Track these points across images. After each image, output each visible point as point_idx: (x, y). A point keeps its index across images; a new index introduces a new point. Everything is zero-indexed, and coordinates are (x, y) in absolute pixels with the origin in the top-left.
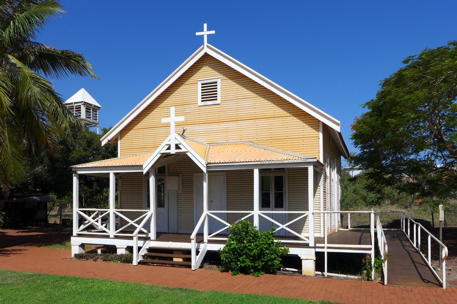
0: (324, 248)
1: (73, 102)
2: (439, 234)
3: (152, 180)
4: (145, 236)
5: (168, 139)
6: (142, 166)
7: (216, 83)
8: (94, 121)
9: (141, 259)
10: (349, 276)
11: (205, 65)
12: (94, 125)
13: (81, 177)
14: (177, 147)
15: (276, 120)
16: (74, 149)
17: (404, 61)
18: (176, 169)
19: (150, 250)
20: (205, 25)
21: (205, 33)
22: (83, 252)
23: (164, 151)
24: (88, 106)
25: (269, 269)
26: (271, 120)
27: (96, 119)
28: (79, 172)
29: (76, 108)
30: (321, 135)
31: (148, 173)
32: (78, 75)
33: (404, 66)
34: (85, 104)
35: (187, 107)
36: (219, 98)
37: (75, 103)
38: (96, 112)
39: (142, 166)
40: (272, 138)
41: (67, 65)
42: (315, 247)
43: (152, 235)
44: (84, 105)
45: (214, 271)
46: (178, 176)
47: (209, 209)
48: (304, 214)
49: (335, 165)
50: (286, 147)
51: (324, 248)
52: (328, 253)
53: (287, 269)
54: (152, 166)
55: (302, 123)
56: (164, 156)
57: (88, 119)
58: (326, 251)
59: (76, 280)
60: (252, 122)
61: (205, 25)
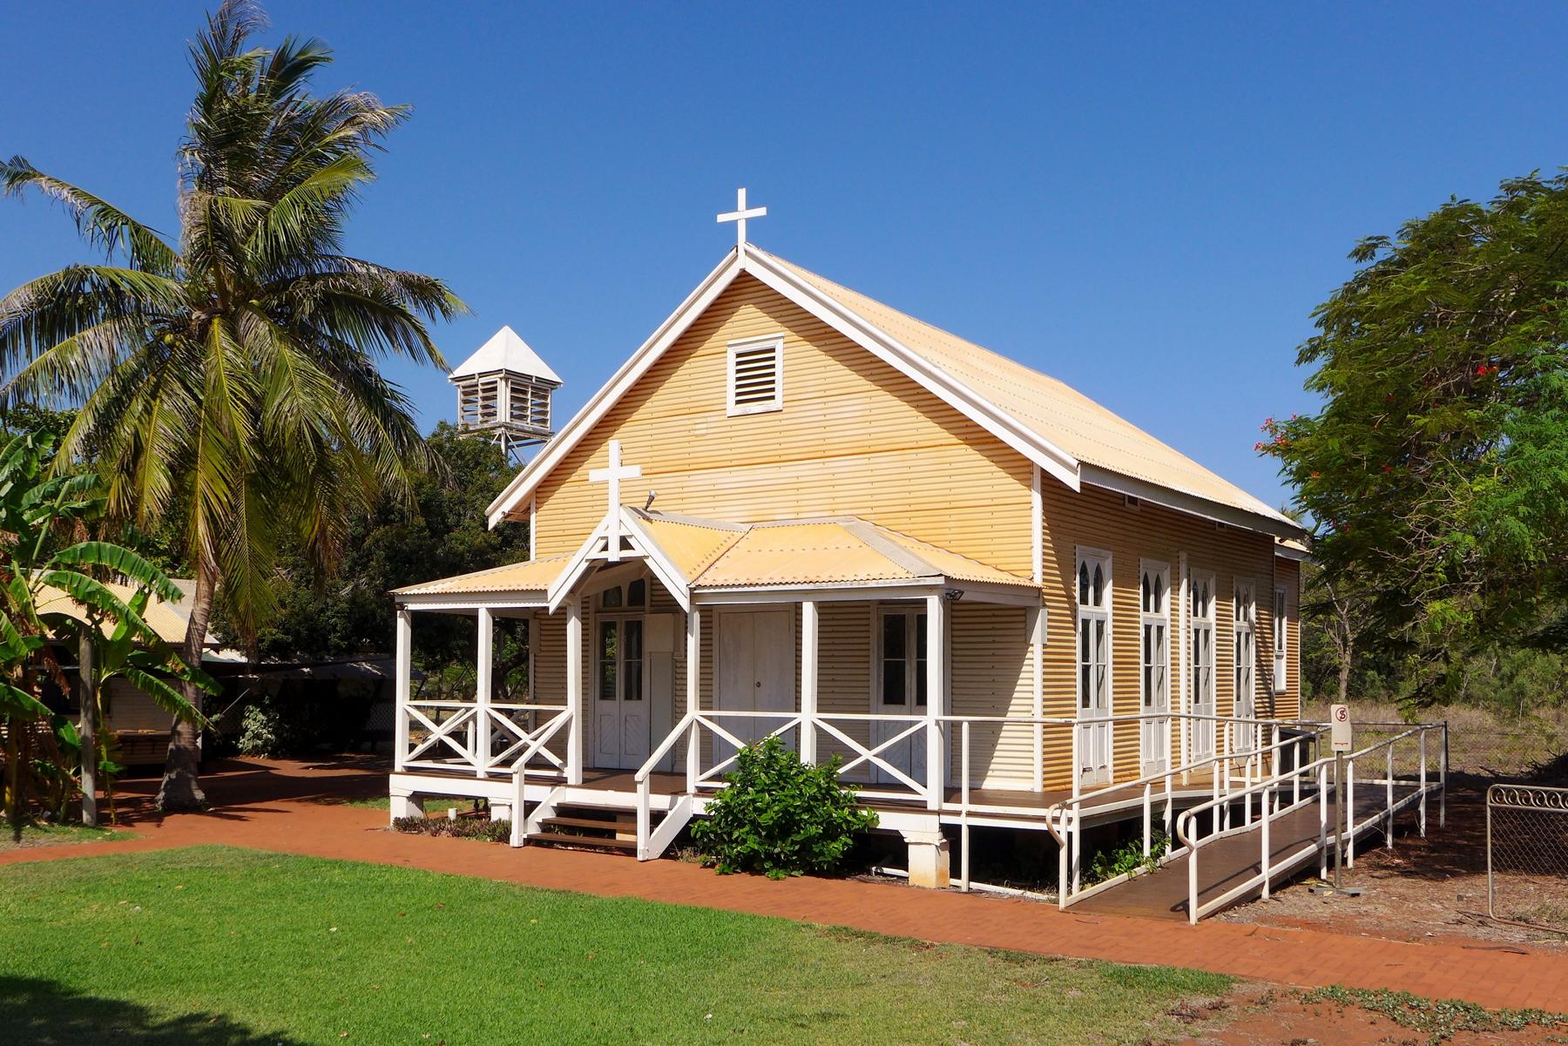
0: (958, 813)
1: (476, 371)
2: (923, 767)
3: (573, 629)
4: (554, 774)
5: (601, 526)
7: (773, 350)
8: (537, 426)
9: (534, 830)
10: (1029, 894)
11: (746, 301)
12: (537, 438)
13: (418, 620)
14: (625, 544)
15: (923, 454)
16: (457, 525)
17: (1356, 253)
18: (624, 600)
19: (563, 810)
20: (742, 194)
21: (742, 214)
22: (418, 814)
23: (596, 554)
24: (520, 384)
25: (808, 863)
26: (910, 455)
27: (545, 421)
29: (484, 391)
30: (1037, 499)
31: (562, 611)
34: (510, 375)
35: (699, 418)
36: (778, 394)
37: (482, 375)
38: (545, 397)
41: (387, 330)
42: (939, 813)
43: (573, 772)
44: (506, 380)
45: (689, 866)
47: (705, 704)
48: (912, 724)
49: (1183, 568)
51: (958, 813)
52: (973, 830)
53: (886, 870)
54: (572, 591)
55: (987, 462)
56: (597, 568)
57: (517, 423)
58: (964, 822)
59: (339, 864)
60: (861, 461)
61: (742, 194)
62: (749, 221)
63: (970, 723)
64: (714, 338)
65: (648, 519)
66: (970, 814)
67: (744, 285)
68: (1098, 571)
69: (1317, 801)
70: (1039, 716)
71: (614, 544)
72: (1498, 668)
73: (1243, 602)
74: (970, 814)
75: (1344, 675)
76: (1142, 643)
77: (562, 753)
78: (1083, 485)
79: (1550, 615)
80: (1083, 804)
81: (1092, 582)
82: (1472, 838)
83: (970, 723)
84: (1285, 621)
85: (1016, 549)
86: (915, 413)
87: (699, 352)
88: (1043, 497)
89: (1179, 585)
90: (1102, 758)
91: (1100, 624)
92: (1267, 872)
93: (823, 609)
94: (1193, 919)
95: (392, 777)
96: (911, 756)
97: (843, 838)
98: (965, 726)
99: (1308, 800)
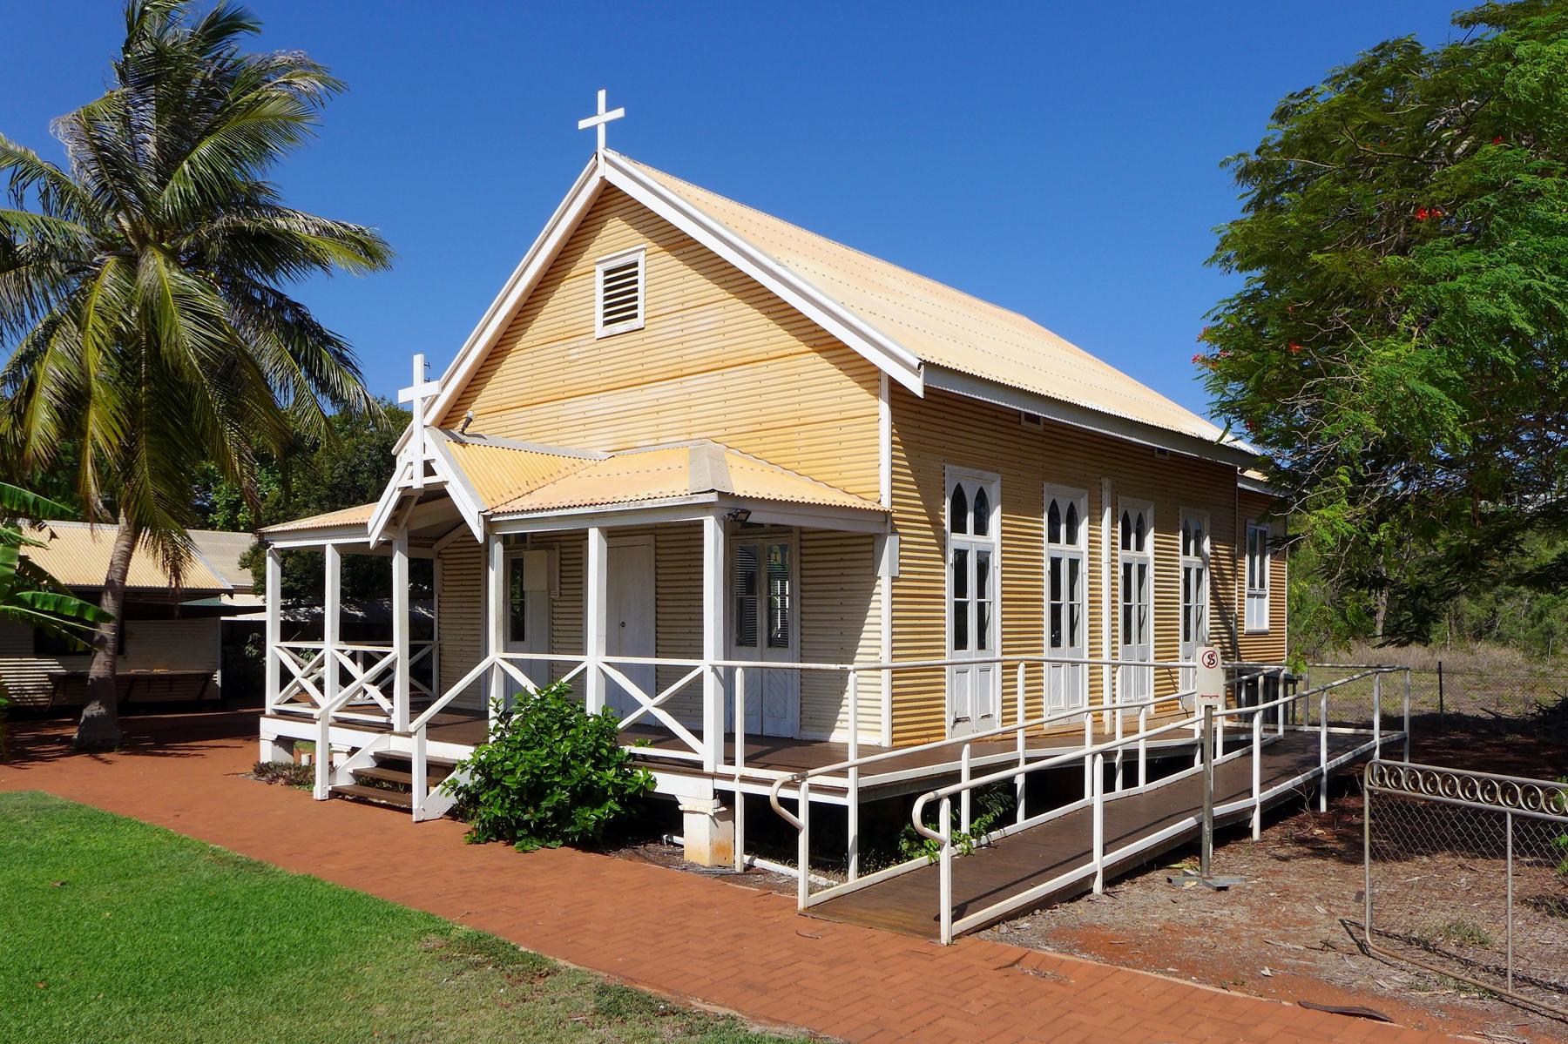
3: (400, 566)
6: (365, 525)
7: (635, 265)
14: (429, 470)
15: (775, 365)
21: (603, 117)
26: (761, 368)
28: (278, 545)
30: (884, 409)
31: (386, 546)
32: (382, 271)
33: (1277, 133)
35: (572, 343)
39: (365, 525)
40: (764, 426)
42: (713, 776)
46: (547, 548)
49: (1106, 496)
50: (796, 451)
58: (739, 788)
60: (715, 377)
62: (609, 125)
63: (745, 669)
64: (585, 257)
65: (462, 443)
66: (744, 779)
67: (607, 197)
68: (1140, 521)
69: (1251, 753)
70: (886, 661)
71: (418, 469)
72: (1529, 609)
73: (1193, 536)
74: (744, 779)
75: (1380, 617)
76: (1181, 585)
77: (388, 692)
78: (927, 390)
79: (1541, 550)
80: (863, 770)
81: (968, 510)
82: (1350, 825)
83: (745, 669)
84: (1268, 558)
85: (852, 463)
86: (766, 320)
87: (573, 273)
88: (892, 407)
89: (1101, 514)
90: (985, 704)
91: (1142, 568)
92: (1099, 862)
93: (610, 534)
94: (945, 937)
95: (263, 720)
96: (688, 706)
97: (611, 803)
98: (739, 672)
99: (1237, 753)
